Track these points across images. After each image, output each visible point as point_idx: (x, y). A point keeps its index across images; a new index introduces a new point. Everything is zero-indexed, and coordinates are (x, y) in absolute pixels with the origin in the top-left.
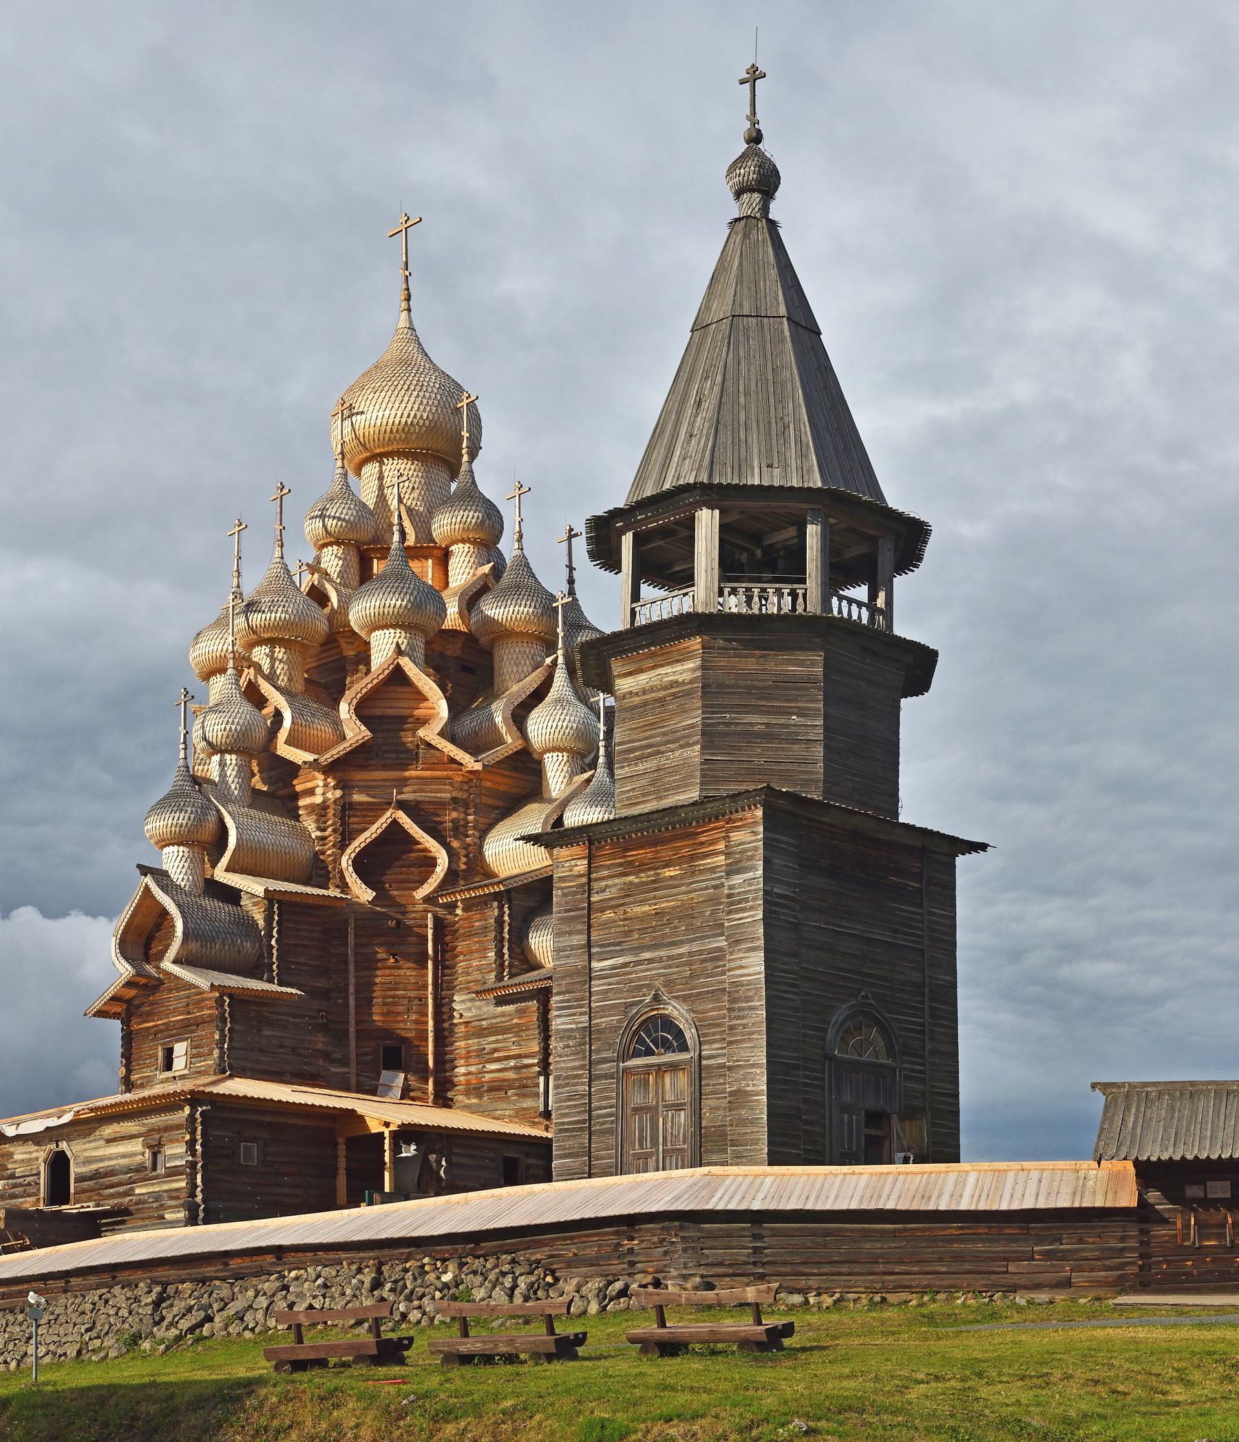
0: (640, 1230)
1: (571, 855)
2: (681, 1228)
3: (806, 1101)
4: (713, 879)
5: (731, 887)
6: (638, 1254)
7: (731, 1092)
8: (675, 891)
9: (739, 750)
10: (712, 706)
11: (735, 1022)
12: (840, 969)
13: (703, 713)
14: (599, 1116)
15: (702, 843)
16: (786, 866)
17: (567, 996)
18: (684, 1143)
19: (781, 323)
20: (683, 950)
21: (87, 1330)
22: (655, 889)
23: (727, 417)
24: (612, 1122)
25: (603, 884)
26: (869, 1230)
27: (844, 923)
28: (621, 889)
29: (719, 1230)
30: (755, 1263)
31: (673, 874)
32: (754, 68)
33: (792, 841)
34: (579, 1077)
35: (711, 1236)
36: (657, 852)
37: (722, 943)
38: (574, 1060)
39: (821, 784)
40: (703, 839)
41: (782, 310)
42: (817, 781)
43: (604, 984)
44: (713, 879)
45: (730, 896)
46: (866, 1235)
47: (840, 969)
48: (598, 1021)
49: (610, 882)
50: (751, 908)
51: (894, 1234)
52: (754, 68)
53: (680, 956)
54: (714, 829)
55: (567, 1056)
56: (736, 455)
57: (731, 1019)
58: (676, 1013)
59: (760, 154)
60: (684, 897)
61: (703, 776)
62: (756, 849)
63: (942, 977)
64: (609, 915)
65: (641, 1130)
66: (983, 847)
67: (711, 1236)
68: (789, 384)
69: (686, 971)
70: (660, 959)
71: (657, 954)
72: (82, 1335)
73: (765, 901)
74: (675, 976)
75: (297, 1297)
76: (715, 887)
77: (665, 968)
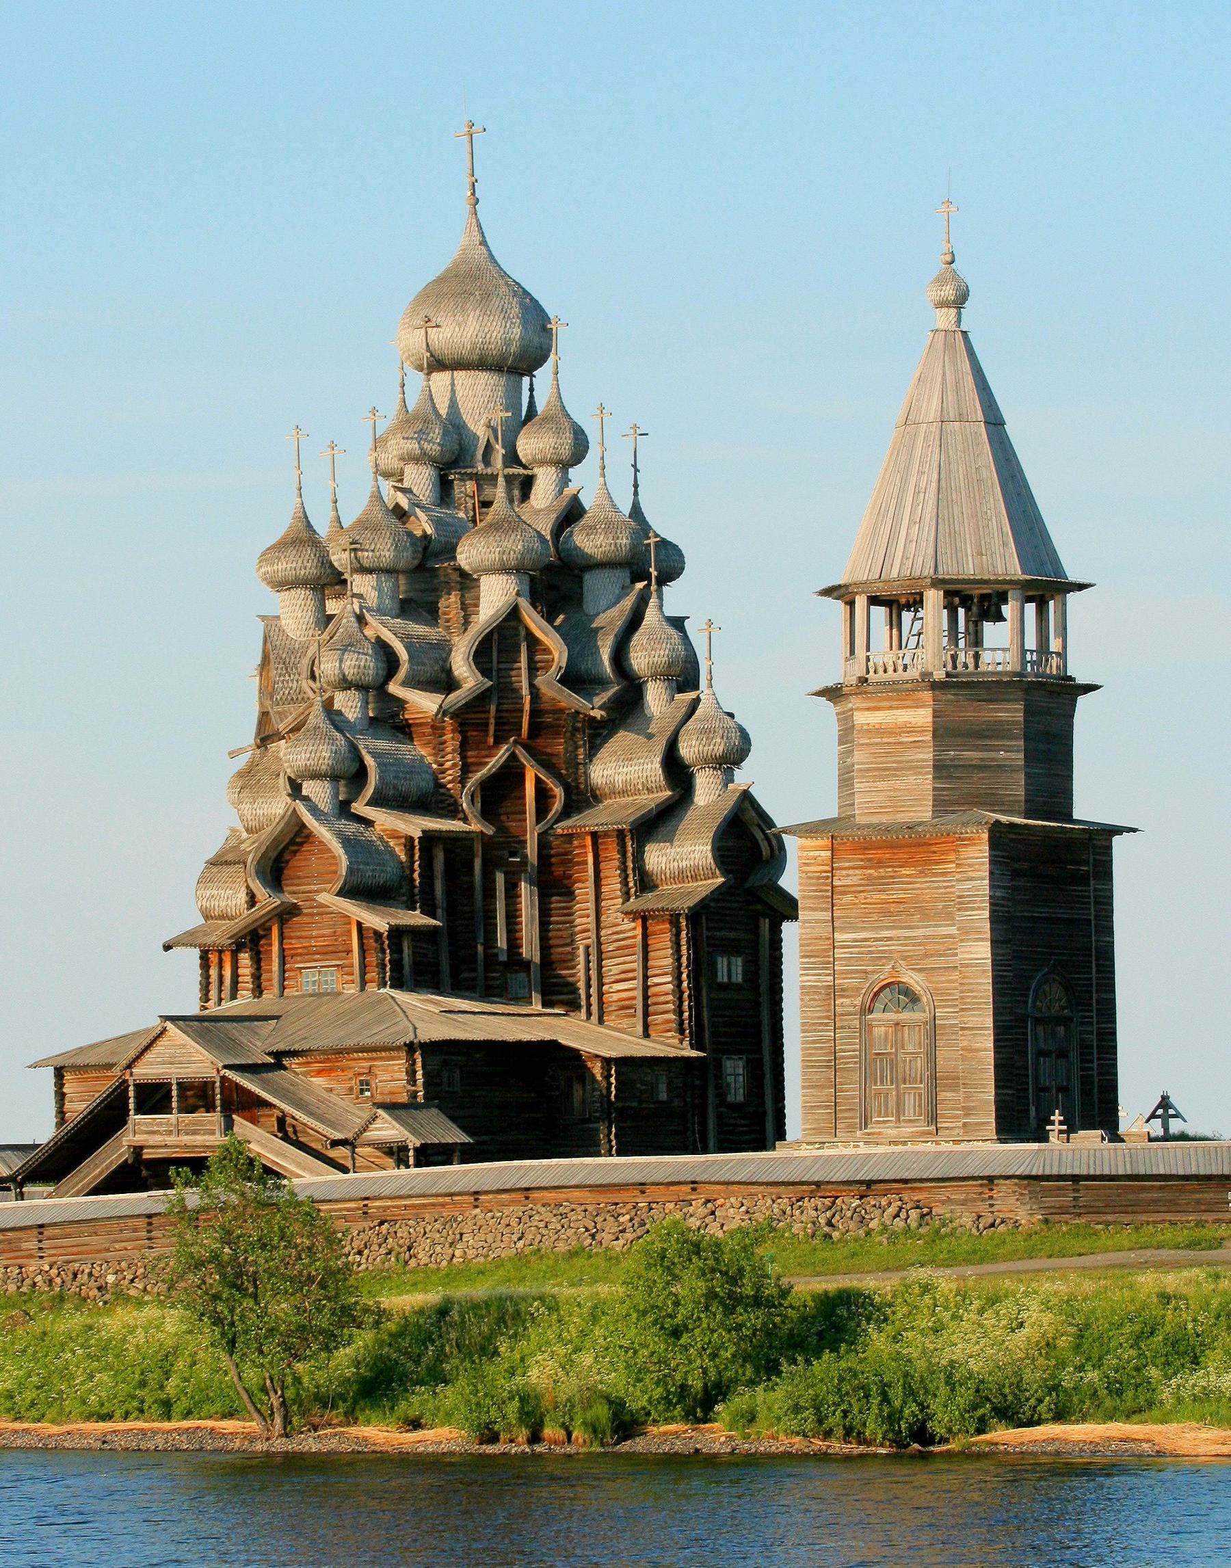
0: (997, 1185)
2: (1029, 1185)
4: (944, 881)
6: (996, 1200)
8: (910, 886)
10: (940, 746)
13: (934, 751)
14: (843, 1057)
15: (935, 852)
18: (921, 1083)
19: (979, 426)
21: (520, 1239)
23: (944, 513)
24: (856, 1062)
25: (844, 872)
26: (1145, 1186)
29: (1051, 1186)
30: (1074, 1206)
31: (908, 873)
33: (1004, 854)
34: (826, 1025)
35: (1044, 1189)
37: (953, 930)
39: (1023, 804)
41: (980, 416)
42: (1019, 801)
44: (944, 881)
46: (1143, 1188)
48: (841, 981)
50: (979, 908)
51: (1161, 1188)
54: (943, 843)
56: (953, 545)
57: (962, 992)
58: (911, 982)
59: (955, 276)
61: (934, 800)
62: (983, 864)
64: (849, 898)
65: (882, 1071)
66: (1135, 830)
67: (1044, 1189)
68: (990, 481)
72: (515, 1243)
73: (991, 904)
75: (724, 1219)
77: (901, 945)
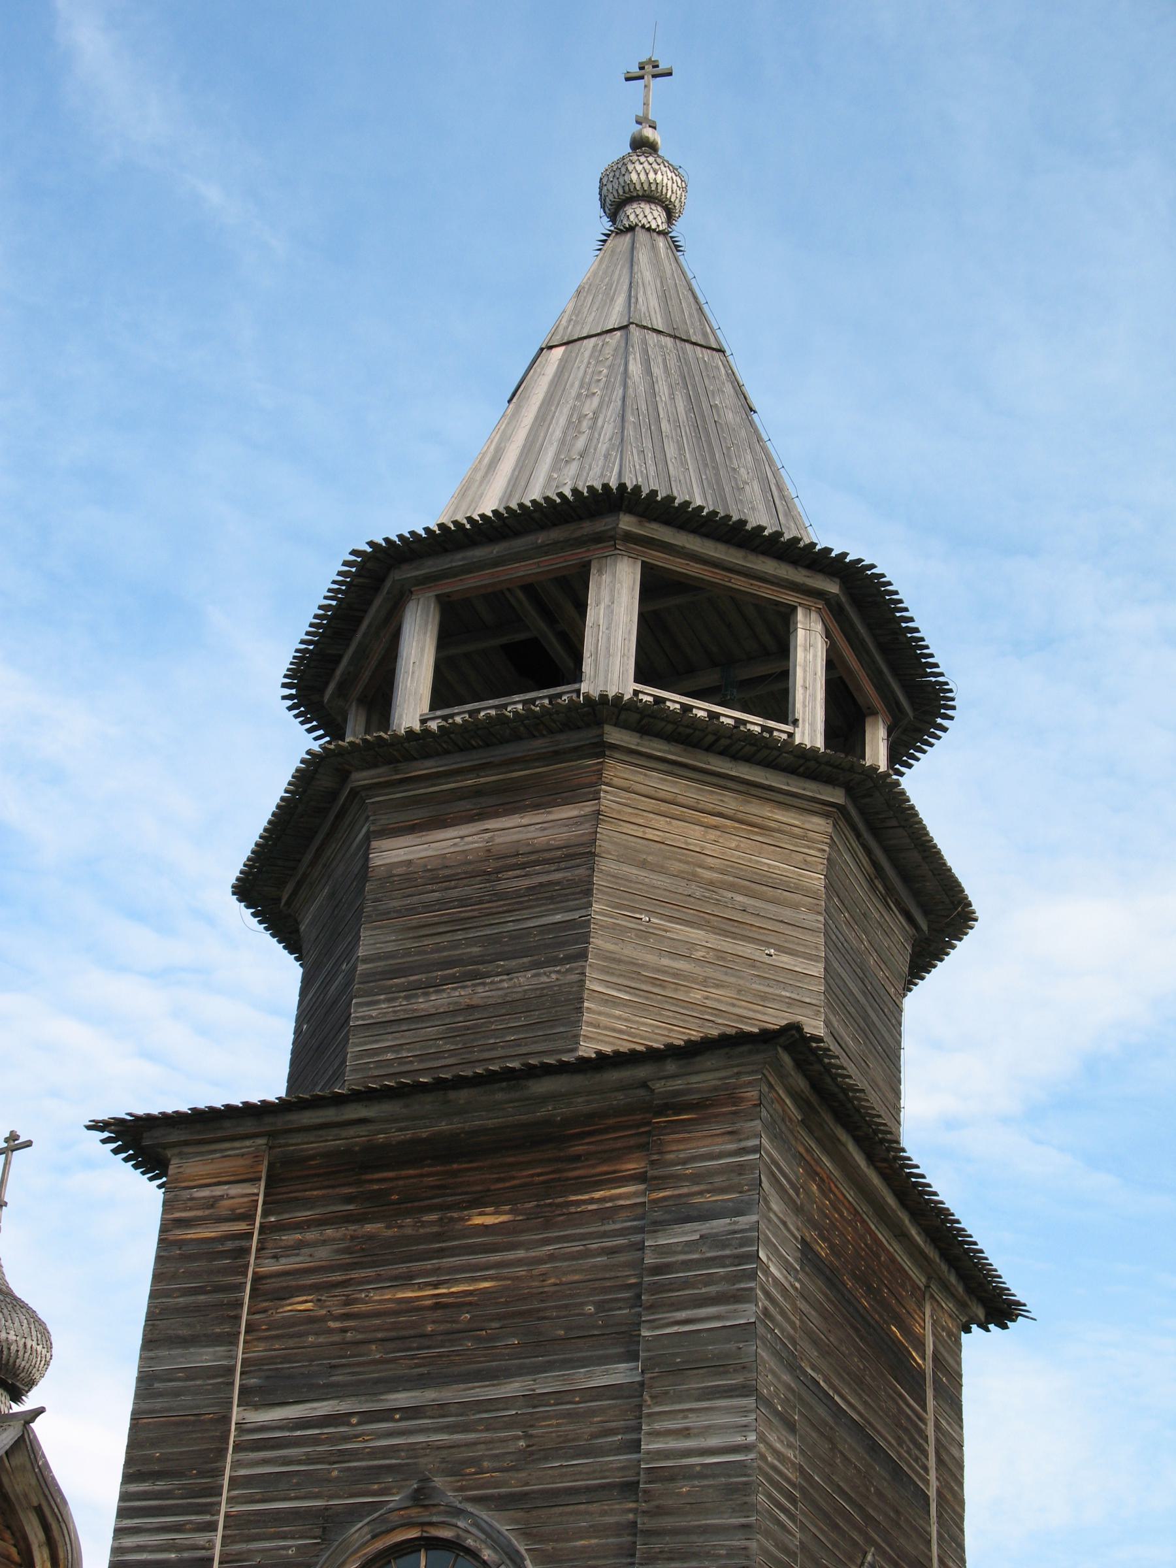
1: (209, 1176)
5: (660, 1250)
9: (664, 987)
12: (842, 1493)
15: (577, 1158)
16: (784, 1223)
17: (160, 1485)
20: (513, 1388)
22: (441, 1253)
27: (845, 1391)
28: (338, 1251)
31: (489, 1220)
32: (13, 1137)
36: (454, 1174)
40: (579, 1149)
45: (658, 1270)
47: (842, 1493)
49: (311, 1235)
52: (13, 1137)
53: (507, 1402)
60: (520, 1271)
66: (1035, 1320)
69: (518, 1438)
70: (442, 1409)
71: (428, 1396)
74: (480, 1451)
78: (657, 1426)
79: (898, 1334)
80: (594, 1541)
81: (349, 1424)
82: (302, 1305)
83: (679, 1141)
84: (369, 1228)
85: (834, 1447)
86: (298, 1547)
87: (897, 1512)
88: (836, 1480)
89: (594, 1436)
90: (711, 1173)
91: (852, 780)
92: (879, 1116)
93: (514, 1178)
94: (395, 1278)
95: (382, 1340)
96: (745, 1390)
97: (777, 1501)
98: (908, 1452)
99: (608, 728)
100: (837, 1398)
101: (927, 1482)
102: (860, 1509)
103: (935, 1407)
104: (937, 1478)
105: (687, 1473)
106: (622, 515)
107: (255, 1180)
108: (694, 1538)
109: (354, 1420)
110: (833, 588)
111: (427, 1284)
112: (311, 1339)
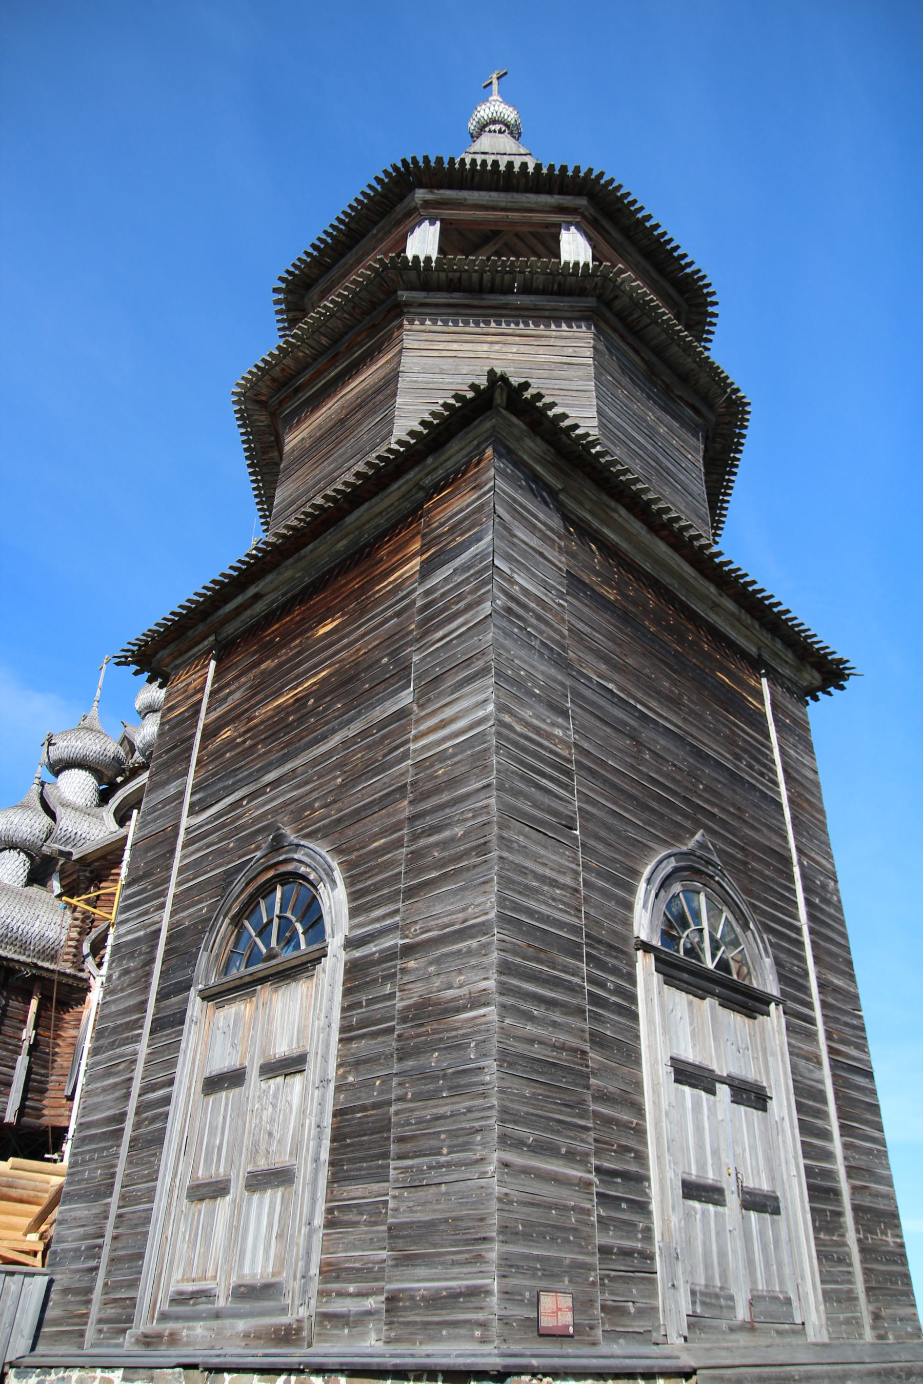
3: (598, 1041)
7: (407, 1008)
11: (423, 842)
38: (130, 995)
43: (198, 850)
55: (122, 990)
57: (415, 837)
63: (813, 855)
76: (398, 614)
78: (423, 727)
79: (727, 680)
80: (383, 841)
81: (242, 806)
82: (227, 733)
83: (439, 513)
84: (263, 666)
85: (639, 743)
86: (207, 906)
87: (739, 809)
88: (645, 770)
89: (385, 756)
90: (461, 522)
91: (596, 284)
92: (627, 471)
93: (344, 592)
94: (275, 693)
95: (265, 739)
96: (485, 671)
97: (532, 766)
98: (751, 767)
99: (400, 293)
100: (639, 706)
101: (779, 794)
102: (685, 800)
103: (778, 738)
104: (787, 789)
105: (442, 757)
106: (417, 190)
107: (721, 911)
108: (447, 811)
109: (245, 803)
110: (582, 202)
111: (290, 689)
112: (228, 755)
